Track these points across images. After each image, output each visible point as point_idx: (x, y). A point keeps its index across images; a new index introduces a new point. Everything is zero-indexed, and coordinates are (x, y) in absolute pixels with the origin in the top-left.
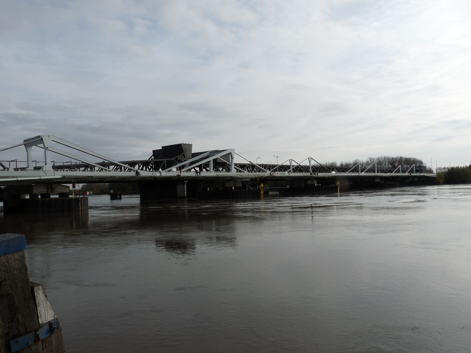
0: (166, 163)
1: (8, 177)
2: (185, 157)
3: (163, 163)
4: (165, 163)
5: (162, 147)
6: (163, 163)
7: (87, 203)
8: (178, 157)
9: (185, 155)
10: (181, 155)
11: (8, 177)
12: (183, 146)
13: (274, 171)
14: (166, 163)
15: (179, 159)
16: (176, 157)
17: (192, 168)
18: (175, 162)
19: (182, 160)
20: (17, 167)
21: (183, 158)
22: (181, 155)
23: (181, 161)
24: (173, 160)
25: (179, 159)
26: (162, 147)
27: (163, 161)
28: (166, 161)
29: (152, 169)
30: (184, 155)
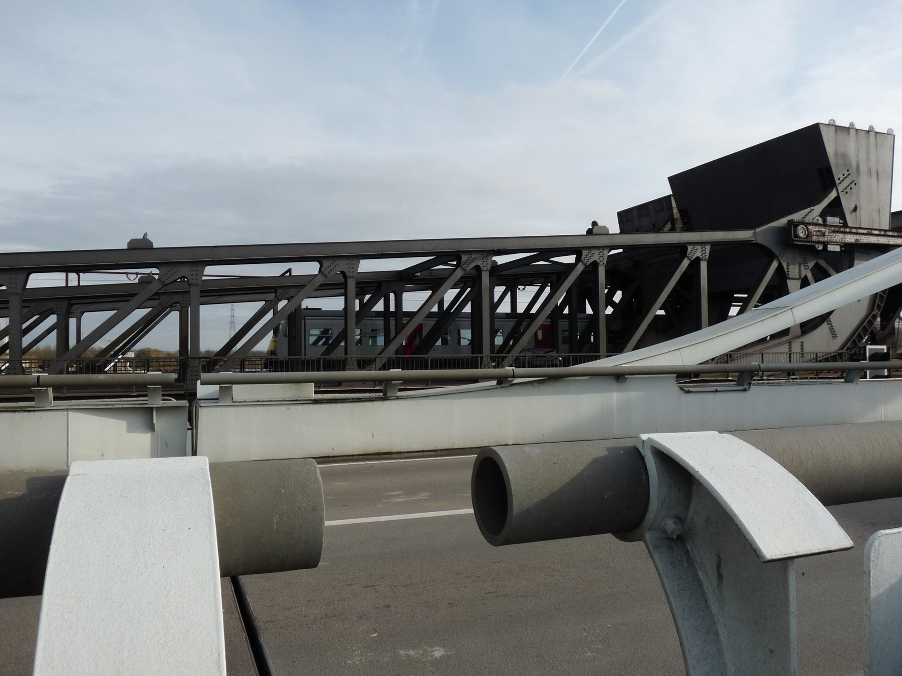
0: (704, 266)
1: (500, 321)
2: (845, 225)
3: (686, 263)
4: (698, 260)
5: (672, 180)
6: (686, 263)
7: (367, 395)
8: (796, 217)
9: (847, 205)
10: (819, 208)
11: (500, 321)
12: (38, 597)
13: (716, 360)
14: (704, 266)
15: (809, 235)
16: (783, 221)
17: (820, 361)
18: (772, 256)
19: (825, 244)
20: (568, 329)
21: (837, 230)
22: (819, 208)
23: (821, 248)
24: (760, 241)
25: (809, 235)
26: (672, 180)
27: (681, 249)
28: (708, 248)
29: (495, 301)
30: (835, 208)
